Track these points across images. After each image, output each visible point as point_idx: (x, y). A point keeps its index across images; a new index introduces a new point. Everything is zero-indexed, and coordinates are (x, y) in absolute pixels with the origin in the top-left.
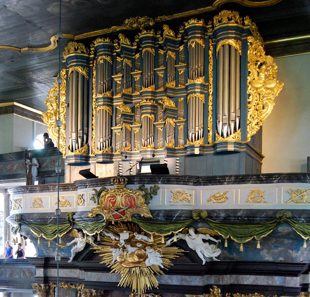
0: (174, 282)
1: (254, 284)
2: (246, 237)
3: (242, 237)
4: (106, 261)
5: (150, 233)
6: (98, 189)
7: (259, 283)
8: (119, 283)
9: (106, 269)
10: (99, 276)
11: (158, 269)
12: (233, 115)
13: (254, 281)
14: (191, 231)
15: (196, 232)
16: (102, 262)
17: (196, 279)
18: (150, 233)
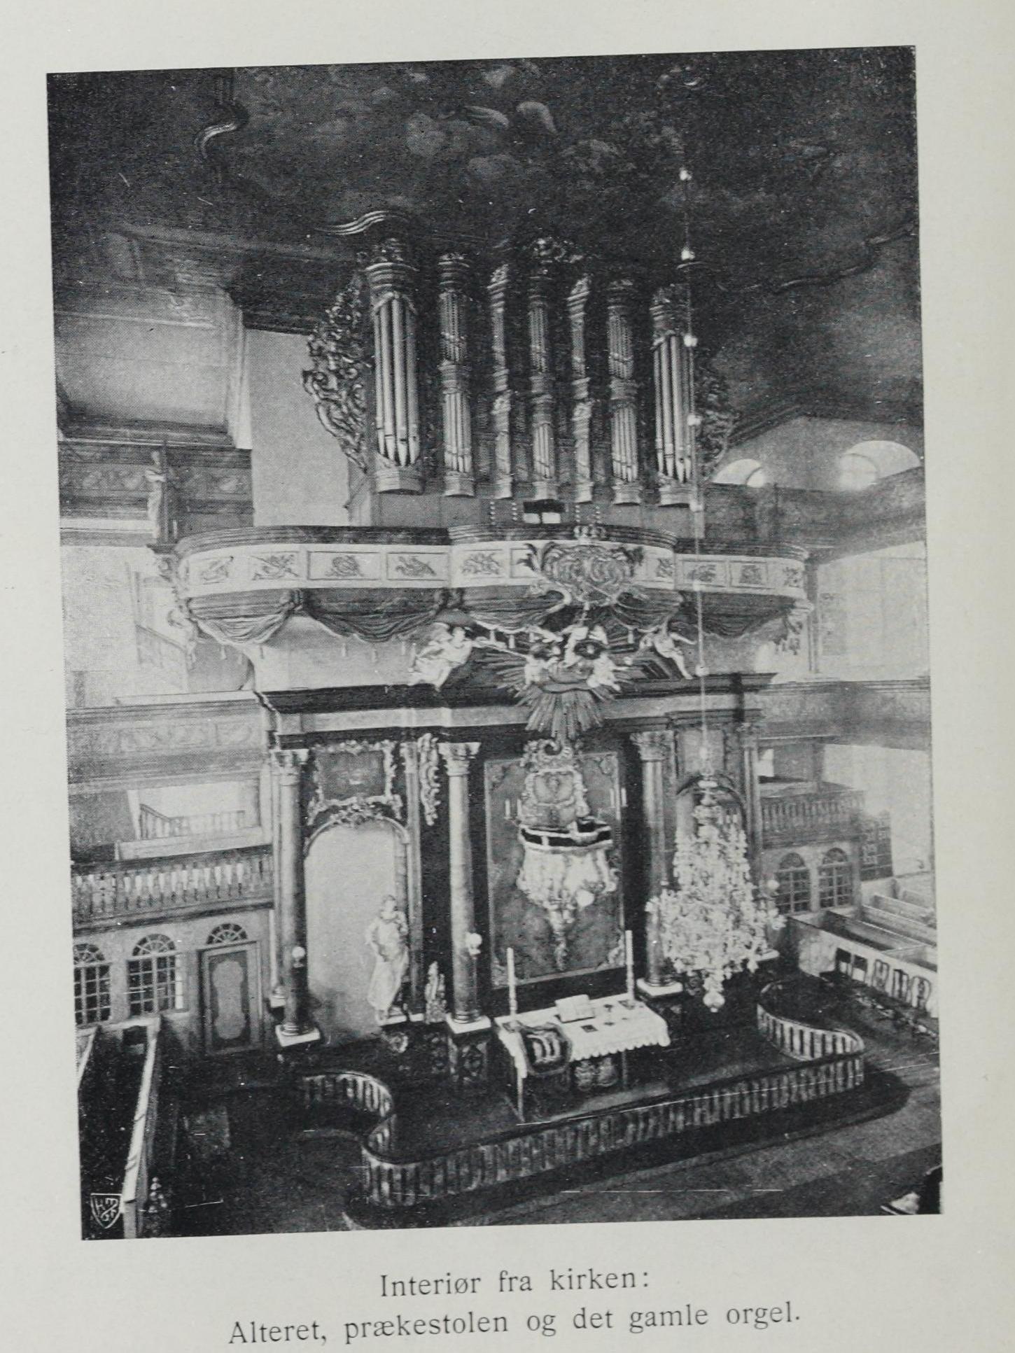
8: (526, 725)
11: (605, 692)
18: (630, 628)
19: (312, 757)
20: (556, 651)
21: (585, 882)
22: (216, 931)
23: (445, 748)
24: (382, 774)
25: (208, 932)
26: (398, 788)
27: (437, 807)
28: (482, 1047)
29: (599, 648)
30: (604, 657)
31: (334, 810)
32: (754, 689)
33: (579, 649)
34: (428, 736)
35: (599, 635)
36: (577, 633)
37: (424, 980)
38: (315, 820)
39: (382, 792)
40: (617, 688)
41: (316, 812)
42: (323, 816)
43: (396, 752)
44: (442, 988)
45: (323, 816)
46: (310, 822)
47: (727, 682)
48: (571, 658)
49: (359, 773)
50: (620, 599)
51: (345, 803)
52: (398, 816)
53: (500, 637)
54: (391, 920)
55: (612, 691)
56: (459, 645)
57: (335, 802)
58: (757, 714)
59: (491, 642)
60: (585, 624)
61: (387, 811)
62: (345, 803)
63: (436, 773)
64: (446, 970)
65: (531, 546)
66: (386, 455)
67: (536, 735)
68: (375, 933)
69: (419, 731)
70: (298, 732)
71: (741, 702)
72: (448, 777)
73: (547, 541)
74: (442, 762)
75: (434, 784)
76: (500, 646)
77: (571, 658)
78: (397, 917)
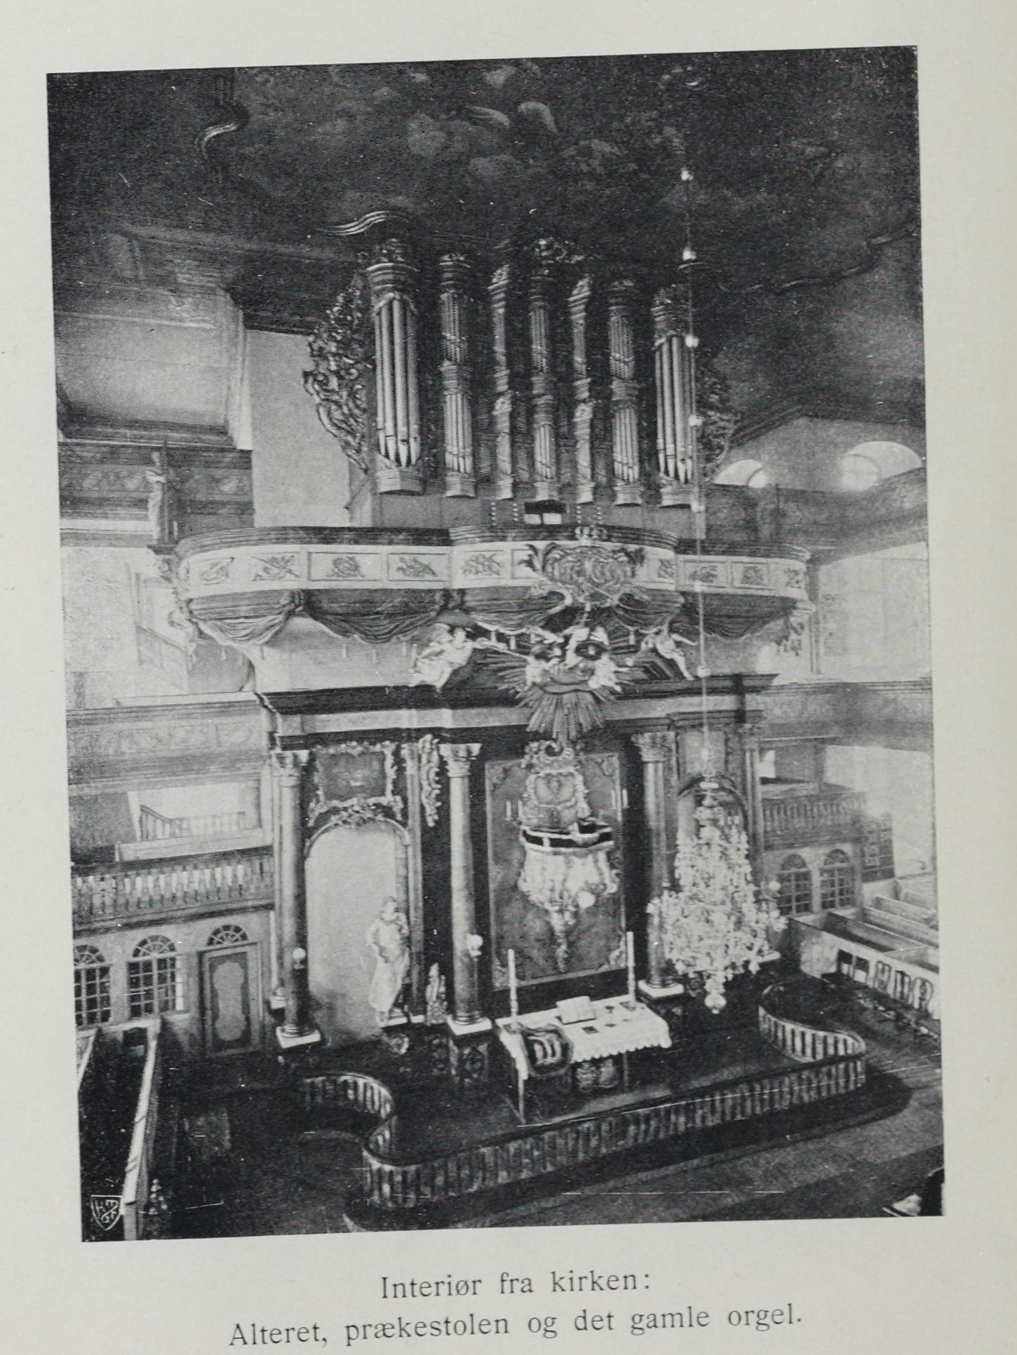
6: (541, 545)
8: (527, 726)
9: (509, 700)
11: (606, 693)
12: (402, 429)
16: (504, 687)
18: (631, 629)
19: (312, 758)
20: (557, 652)
21: (587, 883)
22: (216, 932)
23: (446, 749)
24: (383, 775)
25: (208, 934)
26: (399, 790)
27: (438, 808)
28: (483, 1048)
29: (600, 649)
30: (605, 658)
31: (335, 811)
32: (756, 690)
33: (580, 650)
34: (428, 737)
35: (601, 636)
36: (579, 633)
37: (425, 981)
38: (316, 822)
39: (383, 793)
40: (618, 689)
41: (317, 813)
42: (324, 817)
43: (396, 753)
44: (443, 989)
45: (324, 817)
46: (311, 823)
47: (728, 683)
48: (572, 659)
49: (359, 774)
50: (621, 600)
51: (346, 804)
52: (399, 817)
53: (501, 638)
54: (392, 922)
55: (613, 692)
56: (460, 646)
57: (336, 803)
58: (758, 715)
59: (492, 643)
60: (586, 625)
61: (388, 812)
62: (346, 804)
63: (437, 774)
64: (447, 971)
65: (532, 547)
66: (387, 456)
67: (537, 736)
68: (376, 934)
69: (420, 732)
70: (298, 733)
71: (742, 703)
72: (449, 779)
73: (548, 542)
74: (443, 763)
75: (435, 786)
76: (501, 647)
77: (572, 659)
78: (398, 918)
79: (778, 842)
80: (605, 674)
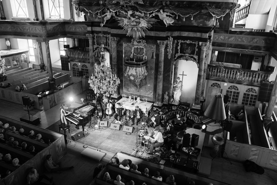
0: (152, 34)
1: (188, 36)
2: (187, 14)
3: (185, 15)
4: (121, 24)
5: (142, 12)
7: (190, 36)
10: (118, 31)
13: (188, 35)
14: (161, 11)
15: (164, 11)
17: (162, 33)
18: (142, 12)
22: (214, 84)
71: (92, 29)
79: (226, 80)
80: (144, 24)
